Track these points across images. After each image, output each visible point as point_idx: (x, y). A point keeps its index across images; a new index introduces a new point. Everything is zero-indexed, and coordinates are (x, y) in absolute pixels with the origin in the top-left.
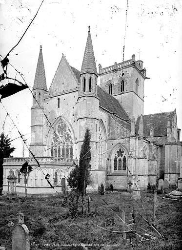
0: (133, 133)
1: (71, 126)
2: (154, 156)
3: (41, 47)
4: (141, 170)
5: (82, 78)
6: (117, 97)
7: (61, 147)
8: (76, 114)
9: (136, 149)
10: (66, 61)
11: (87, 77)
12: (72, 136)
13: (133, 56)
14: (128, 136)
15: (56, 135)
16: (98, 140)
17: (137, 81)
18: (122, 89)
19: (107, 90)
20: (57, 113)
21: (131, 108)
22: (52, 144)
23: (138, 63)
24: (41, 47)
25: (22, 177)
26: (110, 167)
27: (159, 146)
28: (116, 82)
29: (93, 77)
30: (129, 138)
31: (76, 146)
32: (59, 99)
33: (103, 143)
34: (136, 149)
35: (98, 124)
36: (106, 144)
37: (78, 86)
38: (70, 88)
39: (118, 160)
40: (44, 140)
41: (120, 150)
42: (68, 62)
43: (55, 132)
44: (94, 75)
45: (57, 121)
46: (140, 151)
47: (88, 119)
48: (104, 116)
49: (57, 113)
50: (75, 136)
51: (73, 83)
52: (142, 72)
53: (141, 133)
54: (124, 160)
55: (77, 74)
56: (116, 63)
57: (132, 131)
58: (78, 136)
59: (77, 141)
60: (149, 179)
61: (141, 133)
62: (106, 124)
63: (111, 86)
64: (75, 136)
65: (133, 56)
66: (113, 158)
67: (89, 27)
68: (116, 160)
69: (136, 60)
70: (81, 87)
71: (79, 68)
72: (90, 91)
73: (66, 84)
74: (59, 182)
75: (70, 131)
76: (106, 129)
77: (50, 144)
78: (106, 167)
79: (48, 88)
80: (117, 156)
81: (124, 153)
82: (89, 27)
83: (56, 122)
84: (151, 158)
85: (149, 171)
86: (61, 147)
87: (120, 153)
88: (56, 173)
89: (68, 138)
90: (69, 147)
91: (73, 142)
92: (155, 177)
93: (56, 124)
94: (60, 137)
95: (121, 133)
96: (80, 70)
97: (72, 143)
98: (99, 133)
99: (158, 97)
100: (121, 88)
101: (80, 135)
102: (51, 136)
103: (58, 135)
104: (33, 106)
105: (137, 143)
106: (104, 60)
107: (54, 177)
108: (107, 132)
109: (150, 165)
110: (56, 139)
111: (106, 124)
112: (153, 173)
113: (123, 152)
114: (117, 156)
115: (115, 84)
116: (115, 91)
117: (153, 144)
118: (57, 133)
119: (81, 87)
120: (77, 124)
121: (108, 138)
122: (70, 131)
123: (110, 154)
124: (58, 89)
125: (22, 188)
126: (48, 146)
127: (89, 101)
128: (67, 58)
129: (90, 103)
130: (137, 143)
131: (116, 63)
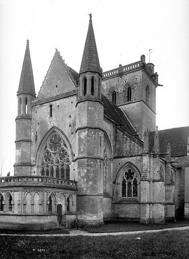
0: (146, 149)
1: (67, 139)
2: (171, 180)
3: (28, 41)
4: (155, 196)
5: (81, 79)
6: (122, 108)
7: (55, 168)
8: (74, 124)
9: (150, 169)
10: (60, 58)
11: (89, 76)
12: (69, 152)
13: (143, 57)
14: (139, 153)
15: (48, 152)
16: (102, 156)
17: (147, 88)
18: (129, 98)
19: (110, 98)
20: (49, 123)
21: (140, 121)
22: (43, 164)
23: (149, 66)
24: (28, 41)
25: (67, 251)
26: (117, 193)
27: (177, 168)
28: (120, 90)
29: (96, 76)
30: (141, 155)
31: (74, 165)
32: (51, 106)
33: (107, 162)
34: (150, 169)
35: (103, 136)
36: (112, 164)
37: (76, 89)
38: (66, 91)
39: (126, 184)
40: (33, 159)
41: (130, 170)
42: (63, 58)
43: (46, 147)
44: (97, 74)
45: (49, 134)
46: (156, 172)
47: (90, 130)
48: (108, 127)
49: (49, 123)
50: (72, 152)
51: (71, 86)
52: (153, 77)
53: (157, 150)
54: (135, 183)
55: (75, 76)
56: (120, 65)
57: (145, 146)
58: (77, 152)
59: (75, 158)
60: (166, 209)
61: (157, 150)
62: (111, 138)
63: (114, 94)
64: (72, 152)
65: (143, 57)
66: (120, 181)
67: (90, 15)
68: (124, 184)
69: (147, 62)
70: (81, 89)
71: (77, 69)
72: (93, 94)
73: (60, 87)
74: (54, 209)
75: (65, 146)
76: (112, 145)
77: (40, 165)
78: (111, 193)
79: (37, 93)
80: (125, 178)
81: (135, 174)
82: (90, 15)
83: (46, 137)
84: (169, 182)
85: (166, 199)
86: (55, 168)
87: (129, 175)
88: (50, 198)
89: (63, 154)
90: (65, 168)
91: (71, 159)
92: (174, 206)
93: (47, 138)
94: (53, 155)
95: (130, 149)
96: (78, 72)
97: (68, 161)
98: (103, 148)
99: (168, 113)
100: (128, 97)
101: (79, 150)
102: (42, 154)
103: (51, 151)
104: (18, 117)
105: (152, 162)
106: (107, 64)
107: (48, 203)
108: (112, 149)
109: (167, 191)
110: (48, 157)
111: (111, 138)
112: (171, 201)
113: (133, 173)
114: (125, 178)
115: (120, 92)
116: (120, 101)
117: (170, 165)
118: (49, 150)
119: (81, 89)
120: (75, 137)
121: (114, 156)
122: (65, 146)
123: (117, 176)
124: (50, 93)
125: (5, 216)
126: (38, 167)
127: (91, 107)
128: (61, 54)
129: (93, 109)
130: (152, 162)
131: (120, 65)
